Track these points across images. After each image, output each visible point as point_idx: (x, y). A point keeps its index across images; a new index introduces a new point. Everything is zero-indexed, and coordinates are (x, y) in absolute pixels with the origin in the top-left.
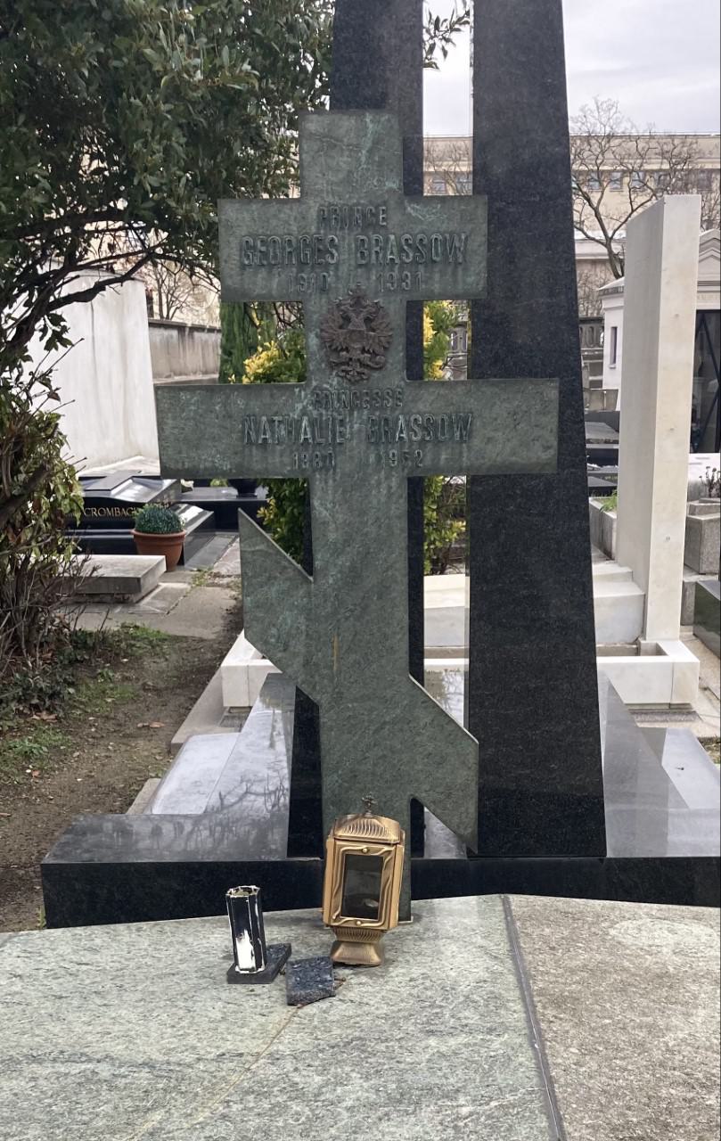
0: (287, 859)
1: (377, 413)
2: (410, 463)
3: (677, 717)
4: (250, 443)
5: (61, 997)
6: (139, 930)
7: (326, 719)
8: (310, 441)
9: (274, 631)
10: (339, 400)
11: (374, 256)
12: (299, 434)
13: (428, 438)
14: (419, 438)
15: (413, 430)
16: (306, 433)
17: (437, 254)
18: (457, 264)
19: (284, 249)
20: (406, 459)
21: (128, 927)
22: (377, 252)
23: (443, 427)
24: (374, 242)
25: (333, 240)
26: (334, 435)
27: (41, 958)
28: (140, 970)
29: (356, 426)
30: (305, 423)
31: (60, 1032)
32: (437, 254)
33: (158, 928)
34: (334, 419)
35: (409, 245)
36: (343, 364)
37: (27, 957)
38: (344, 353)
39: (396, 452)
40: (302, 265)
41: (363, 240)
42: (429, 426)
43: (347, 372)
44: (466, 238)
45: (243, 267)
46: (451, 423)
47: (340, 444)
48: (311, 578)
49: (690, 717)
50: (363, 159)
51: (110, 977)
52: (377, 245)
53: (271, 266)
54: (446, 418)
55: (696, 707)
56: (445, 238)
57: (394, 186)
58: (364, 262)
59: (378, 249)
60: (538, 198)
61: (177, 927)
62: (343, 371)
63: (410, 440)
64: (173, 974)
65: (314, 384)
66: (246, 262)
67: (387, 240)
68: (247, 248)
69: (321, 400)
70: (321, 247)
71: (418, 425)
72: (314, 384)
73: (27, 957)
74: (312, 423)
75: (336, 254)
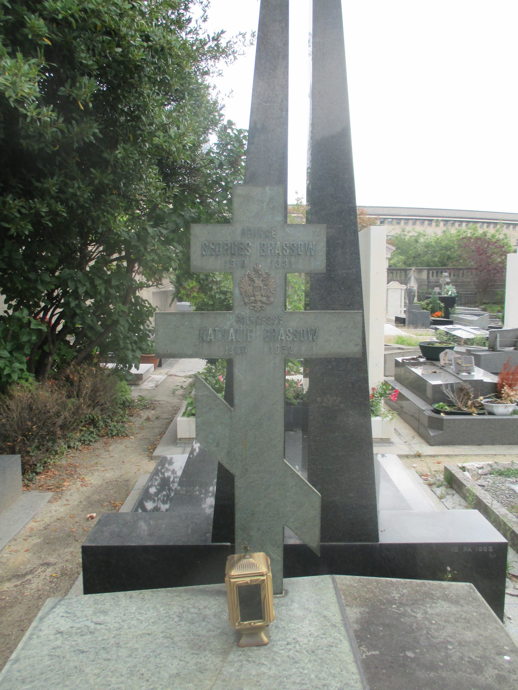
0: (211, 544)
1: (269, 327)
2: (286, 352)
3: (385, 444)
4: (203, 341)
5: (83, 652)
6: (131, 597)
7: (239, 483)
8: (234, 340)
9: (212, 436)
10: (250, 320)
11: (269, 251)
12: (228, 337)
13: (295, 339)
14: (291, 339)
15: (288, 335)
16: (232, 336)
17: (301, 251)
18: (311, 256)
19: (224, 247)
20: (284, 349)
21: (125, 595)
22: (271, 250)
23: (303, 334)
24: (269, 245)
25: (248, 244)
26: (247, 337)
27: (75, 618)
28: (130, 630)
29: (258, 333)
30: (232, 331)
31: (80, 683)
32: (301, 251)
33: (141, 596)
34: (247, 330)
35: (287, 247)
36: (252, 303)
37: (67, 617)
38: (252, 298)
39: (278, 346)
40: (233, 255)
41: (263, 244)
42: (296, 333)
43: (254, 307)
44: (316, 244)
45: (203, 255)
46: (307, 332)
47: (250, 341)
48: (232, 409)
49: (391, 444)
50: (265, 206)
51: (113, 636)
52: (271, 246)
53: (217, 255)
54: (305, 330)
55: (392, 440)
56: (305, 244)
57: (280, 219)
58: (264, 254)
59: (271, 248)
60: (342, 226)
61: (152, 596)
62: (252, 306)
63: (286, 340)
64: (149, 634)
65: (237, 312)
66: (204, 253)
67: (276, 244)
68: (205, 247)
69: (240, 320)
70: (242, 247)
71: (291, 333)
72: (237, 312)
73: (67, 617)
74: (236, 331)
75: (250, 250)
